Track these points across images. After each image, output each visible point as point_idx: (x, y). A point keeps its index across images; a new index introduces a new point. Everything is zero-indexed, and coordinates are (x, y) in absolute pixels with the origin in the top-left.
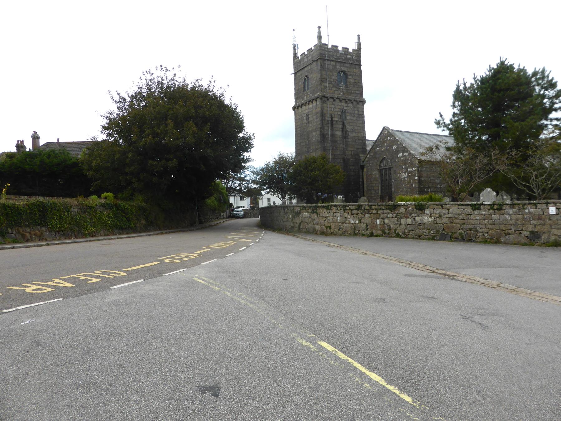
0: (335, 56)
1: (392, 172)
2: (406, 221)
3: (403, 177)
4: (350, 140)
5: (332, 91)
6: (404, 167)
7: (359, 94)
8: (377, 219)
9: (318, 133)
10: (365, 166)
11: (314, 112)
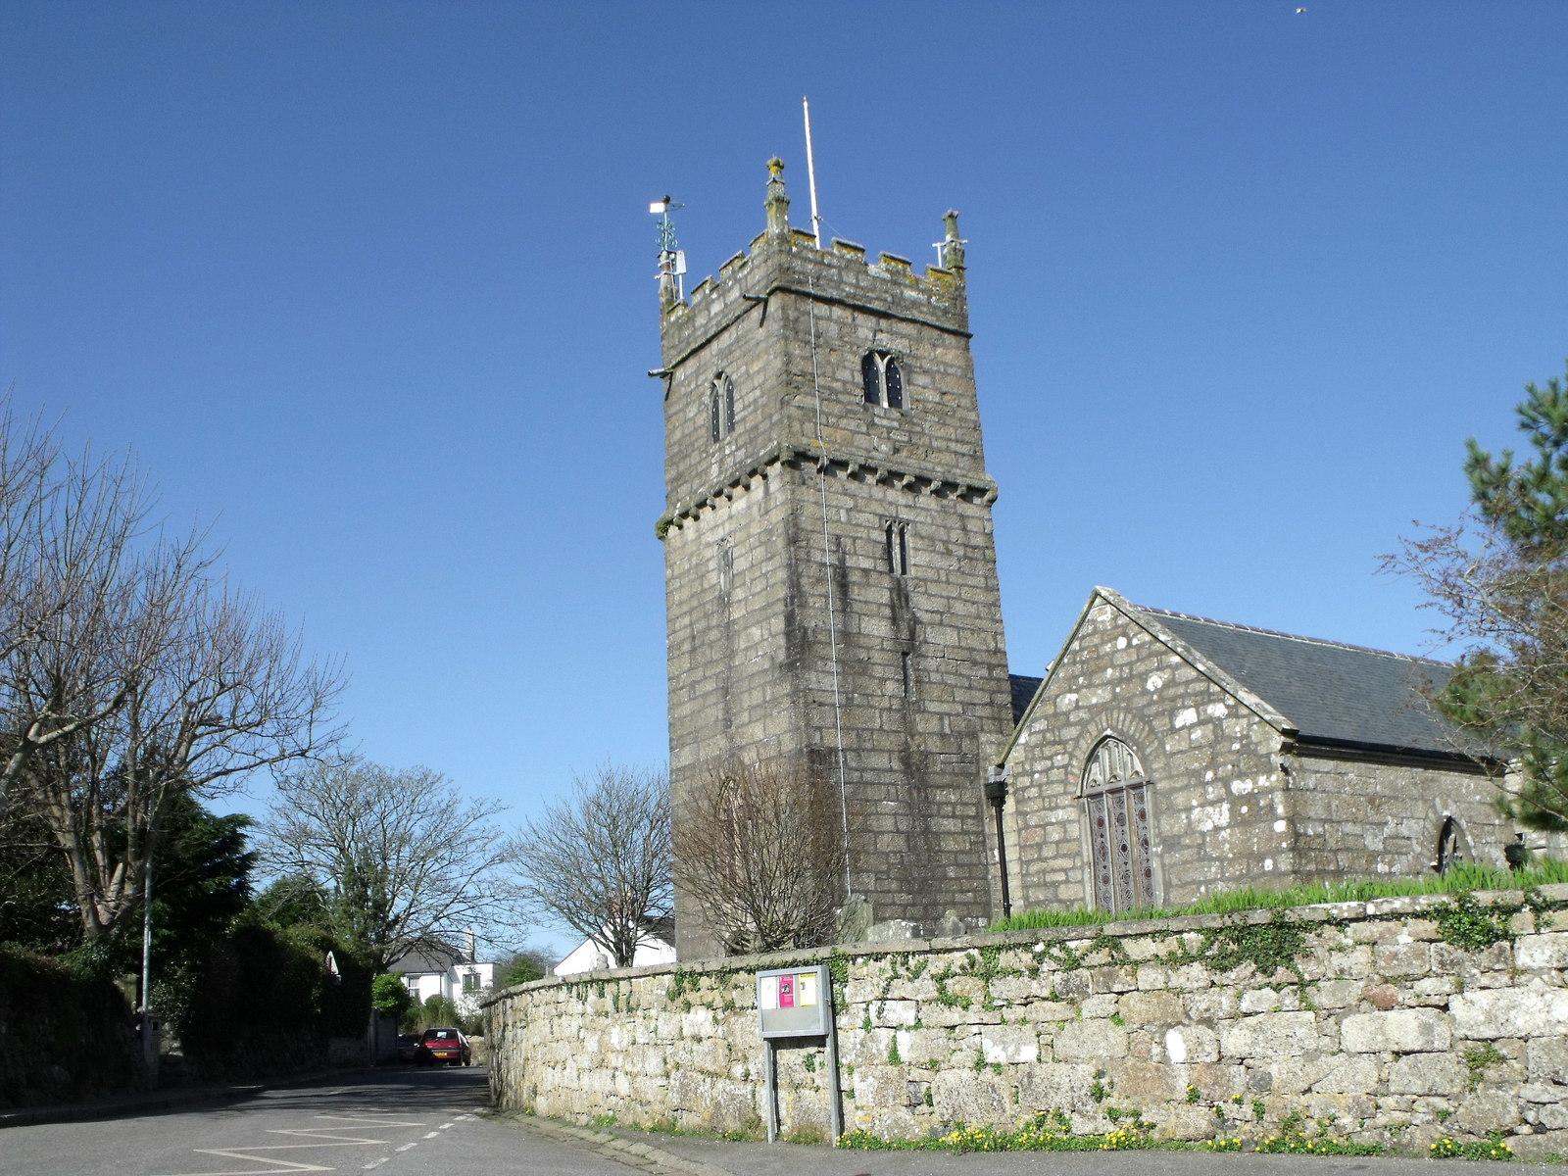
0: (851, 285)
1: (1148, 807)
2: (1381, 1030)
3: (1208, 826)
4: (932, 664)
5: (839, 436)
7: (964, 455)
8: (1170, 1026)
9: (778, 624)
10: (1010, 789)
11: (755, 529)
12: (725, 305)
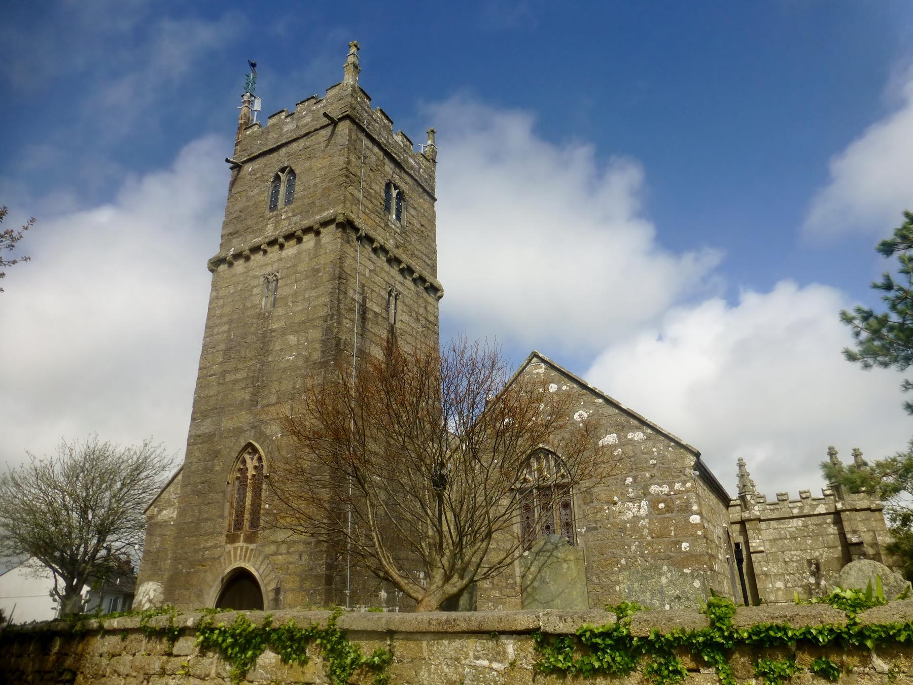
0: (385, 138)
3: (630, 515)
6: (629, 480)
9: (316, 334)
12: (297, 126)
